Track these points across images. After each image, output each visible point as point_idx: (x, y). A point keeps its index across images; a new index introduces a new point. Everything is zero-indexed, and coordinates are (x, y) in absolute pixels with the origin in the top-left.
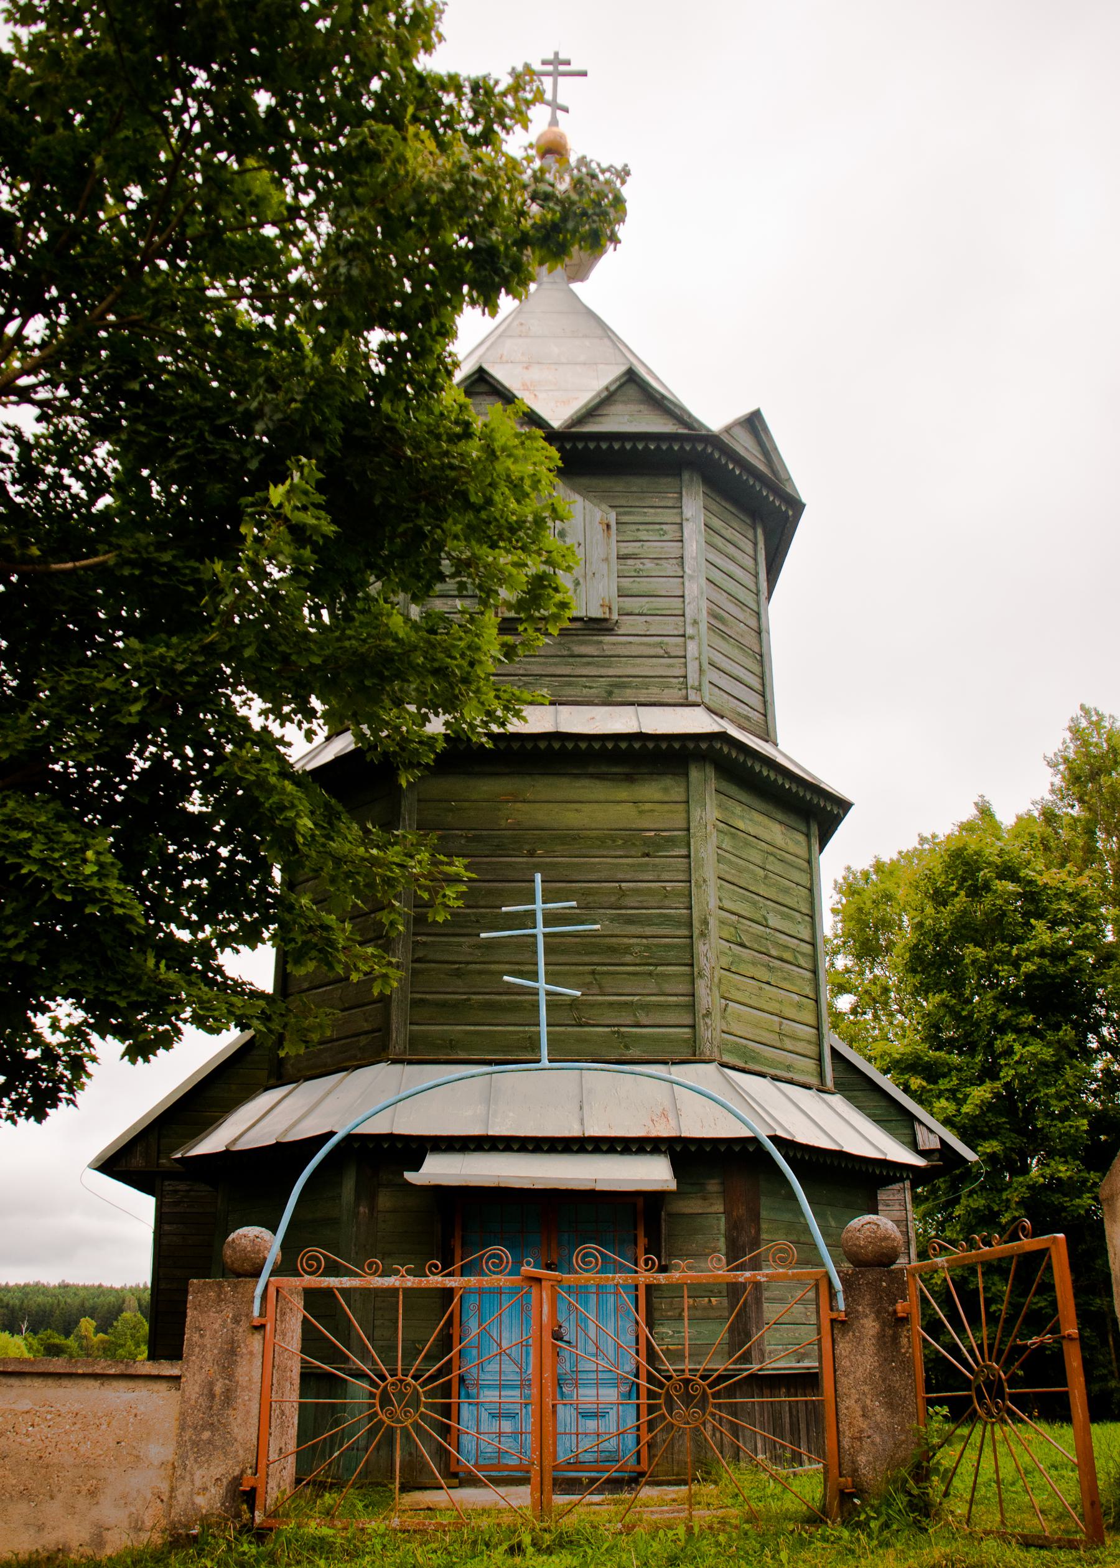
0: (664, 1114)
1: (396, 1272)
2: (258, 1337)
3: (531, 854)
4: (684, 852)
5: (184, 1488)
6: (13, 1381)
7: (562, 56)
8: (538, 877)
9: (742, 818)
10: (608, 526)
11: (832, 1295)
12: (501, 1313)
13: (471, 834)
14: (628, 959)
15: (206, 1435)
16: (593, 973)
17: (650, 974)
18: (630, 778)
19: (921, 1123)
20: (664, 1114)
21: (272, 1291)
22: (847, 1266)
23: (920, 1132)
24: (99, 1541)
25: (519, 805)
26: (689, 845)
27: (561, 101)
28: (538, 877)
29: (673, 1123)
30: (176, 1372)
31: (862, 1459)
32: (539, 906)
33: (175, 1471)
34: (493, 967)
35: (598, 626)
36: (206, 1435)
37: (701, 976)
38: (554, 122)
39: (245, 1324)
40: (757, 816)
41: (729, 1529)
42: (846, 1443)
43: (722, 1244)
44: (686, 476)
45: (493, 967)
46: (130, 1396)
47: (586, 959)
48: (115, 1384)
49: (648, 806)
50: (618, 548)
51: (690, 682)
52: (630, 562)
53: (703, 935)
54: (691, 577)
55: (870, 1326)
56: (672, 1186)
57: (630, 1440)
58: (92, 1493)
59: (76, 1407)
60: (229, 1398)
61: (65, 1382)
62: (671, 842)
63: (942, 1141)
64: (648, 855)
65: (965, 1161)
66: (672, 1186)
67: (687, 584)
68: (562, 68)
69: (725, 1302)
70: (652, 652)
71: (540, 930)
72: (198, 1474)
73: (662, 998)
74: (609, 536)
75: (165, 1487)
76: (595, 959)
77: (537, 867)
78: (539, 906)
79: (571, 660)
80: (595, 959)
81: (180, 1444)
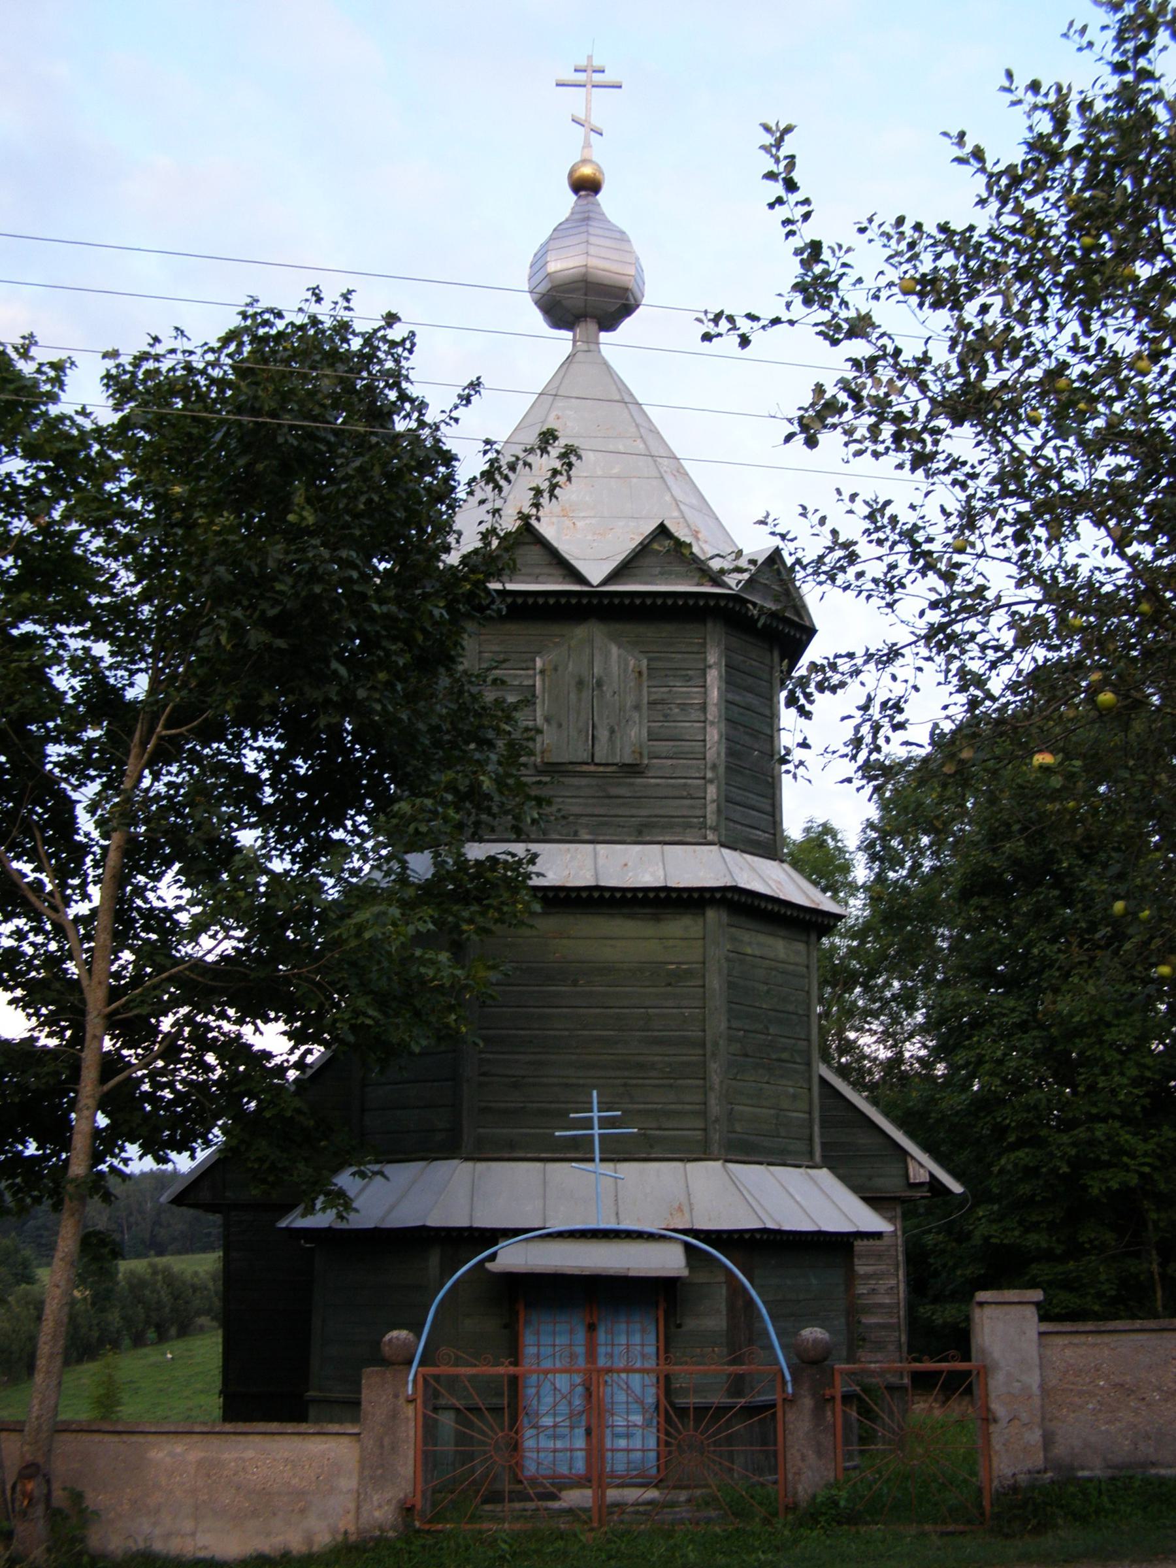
0: (680, 1209)
1: (502, 1364)
2: (411, 1407)
3: (575, 983)
4: (700, 983)
5: (366, 1507)
6: (241, 1438)
7: (597, 63)
8: (595, 1093)
9: (750, 944)
10: (640, 673)
11: (784, 1383)
12: (551, 1353)
13: (524, 966)
14: (653, 1074)
15: (379, 1472)
16: (625, 1085)
17: (671, 1086)
18: (657, 918)
19: (913, 1158)
20: (680, 1209)
21: (420, 1380)
22: (796, 1360)
23: (912, 1166)
24: (309, 1541)
25: (565, 941)
26: (704, 976)
27: (596, 122)
28: (595, 1093)
29: (687, 1216)
30: (356, 1430)
31: (800, 1488)
32: (595, 1114)
33: (360, 1498)
34: (545, 1080)
35: (632, 770)
36: (379, 1472)
37: (712, 1089)
38: (587, 145)
39: (401, 1401)
40: (762, 938)
41: (1117, 1111)
42: (790, 1476)
43: (723, 1307)
44: (710, 625)
45: (545, 1080)
46: (324, 1447)
47: (618, 1073)
48: (313, 1438)
49: (671, 943)
50: (649, 693)
51: (709, 822)
52: (659, 707)
53: (714, 1055)
54: (712, 723)
55: (808, 1402)
56: (685, 1273)
57: (653, 1455)
58: (302, 1511)
59: (286, 1455)
60: (394, 1449)
61: (277, 1438)
62: (689, 973)
63: (931, 1175)
64: (669, 985)
65: (948, 1192)
66: (685, 1273)
67: (708, 729)
68: (597, 78)
69: (725, 1350)
70: (676, 793)
71: (596, 1131)
72: (375, 1498)
73: (680, 1107)
74: (640, 685)
75: (352, 1506)
76: (626, 1074)
77: (594, 1087)
78: (595, 1114)
79: (607, 801)
80: (626, 1074)
81: (361, 1478)
